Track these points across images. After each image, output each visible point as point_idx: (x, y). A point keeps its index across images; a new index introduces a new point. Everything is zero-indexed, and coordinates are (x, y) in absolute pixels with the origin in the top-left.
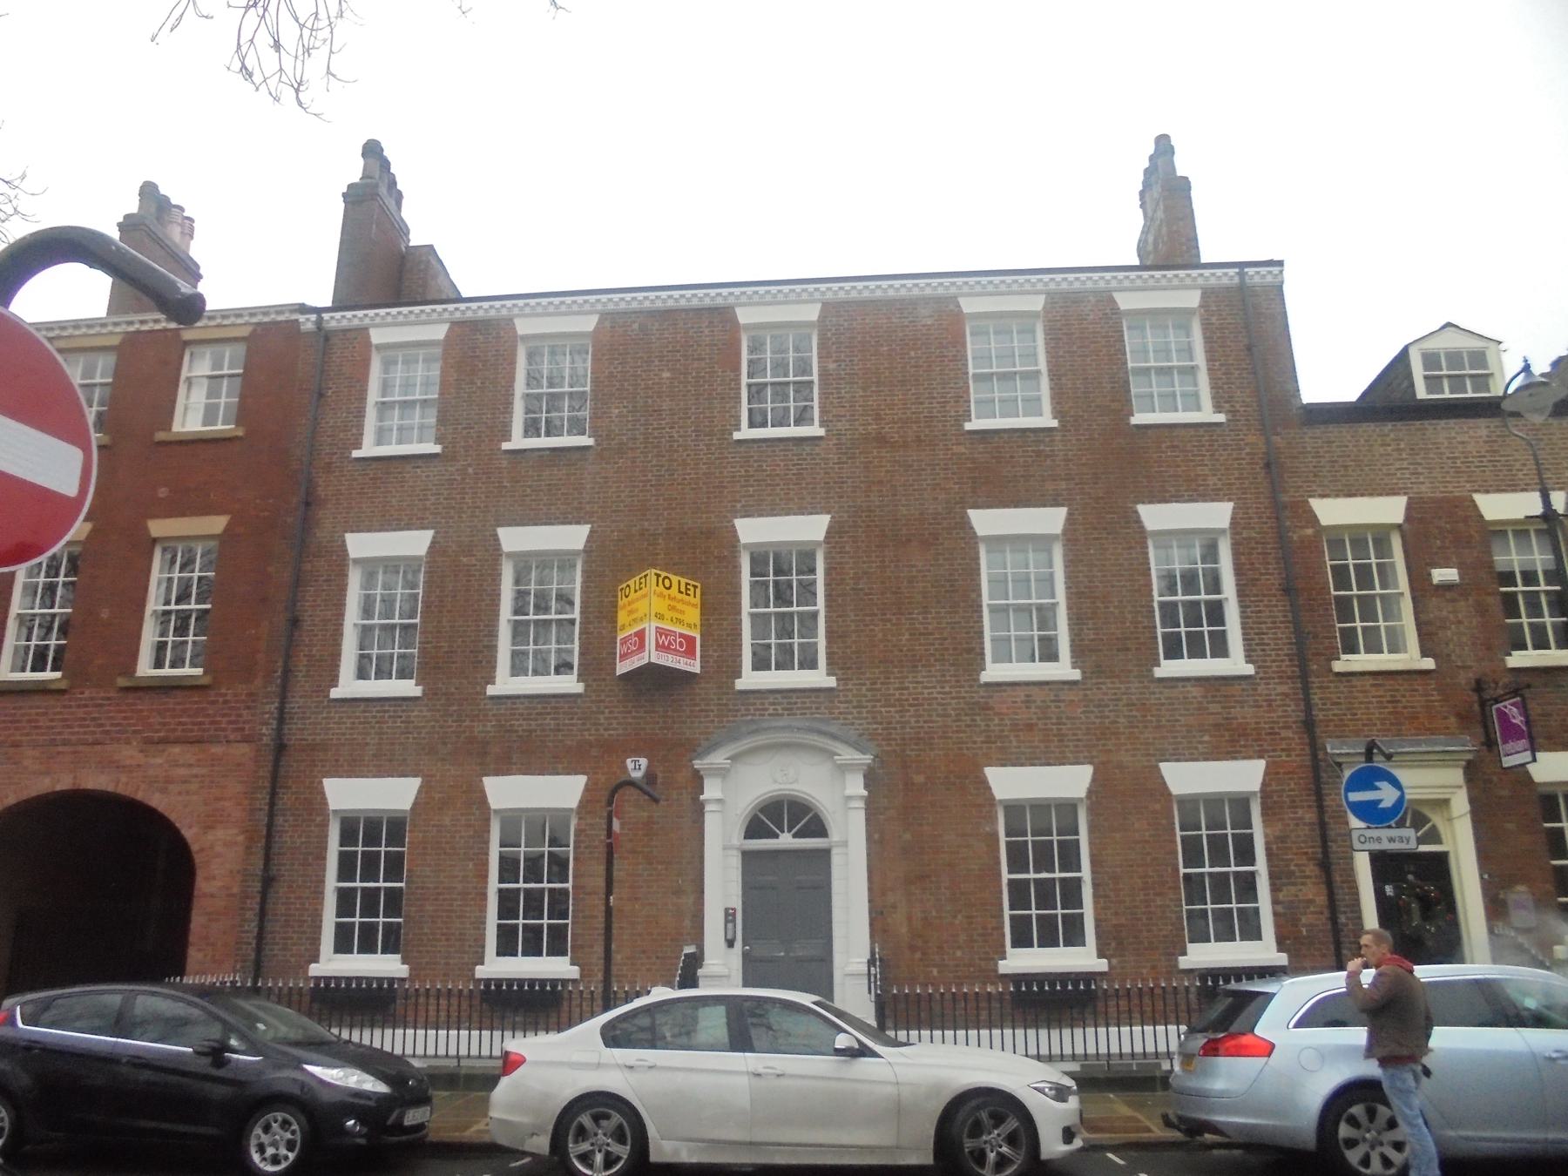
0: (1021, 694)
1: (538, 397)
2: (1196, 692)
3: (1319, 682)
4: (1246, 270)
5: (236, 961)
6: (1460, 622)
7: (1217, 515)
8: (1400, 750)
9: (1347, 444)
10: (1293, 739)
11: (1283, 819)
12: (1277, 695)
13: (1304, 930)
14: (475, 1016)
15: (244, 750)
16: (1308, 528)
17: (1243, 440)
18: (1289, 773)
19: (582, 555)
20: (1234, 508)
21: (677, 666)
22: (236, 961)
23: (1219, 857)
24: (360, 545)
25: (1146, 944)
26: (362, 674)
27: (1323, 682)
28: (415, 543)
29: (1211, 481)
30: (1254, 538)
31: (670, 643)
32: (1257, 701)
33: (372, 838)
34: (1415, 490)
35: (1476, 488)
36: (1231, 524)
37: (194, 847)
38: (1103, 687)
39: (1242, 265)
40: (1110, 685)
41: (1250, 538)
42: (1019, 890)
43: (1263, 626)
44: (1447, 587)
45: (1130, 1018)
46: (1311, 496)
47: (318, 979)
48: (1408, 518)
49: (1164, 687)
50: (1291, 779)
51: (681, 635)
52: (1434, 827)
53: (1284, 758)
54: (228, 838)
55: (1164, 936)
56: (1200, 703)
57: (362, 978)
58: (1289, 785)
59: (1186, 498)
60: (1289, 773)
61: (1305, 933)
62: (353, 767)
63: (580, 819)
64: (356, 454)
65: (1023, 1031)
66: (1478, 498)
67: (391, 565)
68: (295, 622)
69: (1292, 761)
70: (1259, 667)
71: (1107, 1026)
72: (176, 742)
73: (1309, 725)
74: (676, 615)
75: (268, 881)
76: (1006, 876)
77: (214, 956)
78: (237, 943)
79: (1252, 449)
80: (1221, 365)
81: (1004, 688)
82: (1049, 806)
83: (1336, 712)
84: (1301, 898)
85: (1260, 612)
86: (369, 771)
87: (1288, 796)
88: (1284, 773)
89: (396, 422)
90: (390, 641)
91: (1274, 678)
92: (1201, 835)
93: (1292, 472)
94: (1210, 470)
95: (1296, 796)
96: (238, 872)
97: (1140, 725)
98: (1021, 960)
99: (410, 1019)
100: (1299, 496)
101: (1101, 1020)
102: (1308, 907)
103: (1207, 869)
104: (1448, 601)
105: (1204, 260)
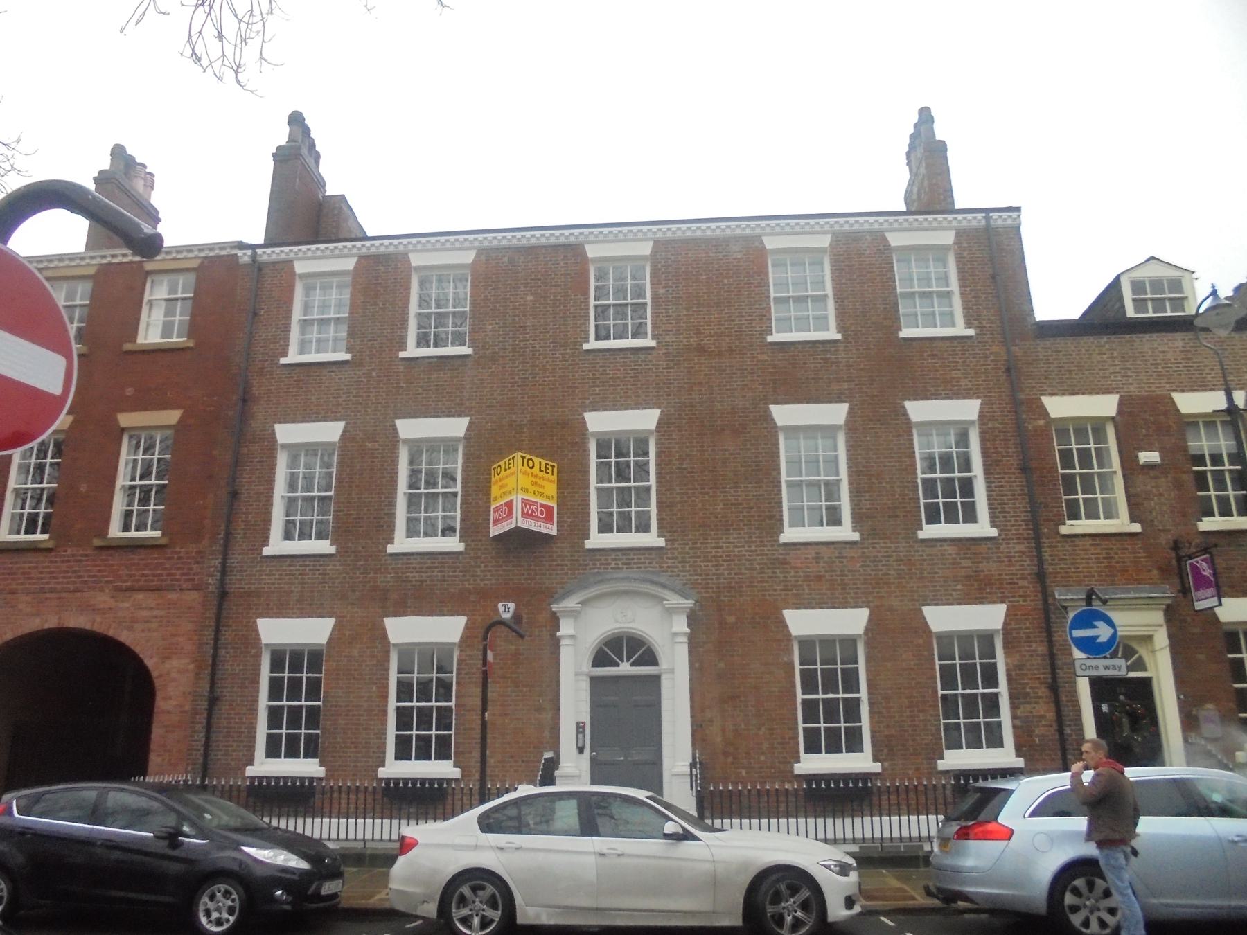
0: (812, 552)
1: (428, 316)
2: (951, 550)
3: (1049, 542)
4: (991, 215)
5: (188, 764)
6: (1161, 495)
7: (968, 409)
8: (1113, 596)
9: (1071, 353)
10: (1029, 587)
11: (1020, 651)
12: (1016, 552)
13: (1037, 739)
14: (378, 808)
15: (194, 596)
16: (1040, 420)
17: (988, 350)
18: (1025, 614)
19: (463, 441)
20: (981, 404)
21: (539, 530)
22: (188, 764)
23: (970, 681)
24: (286, 433)
25: (912, 751)
26: (288, 536)
27: (1052, 542)
28: (330, 431)
29: (963, 382)
30: (998, 428)
31: (533, 511)
32: (1000, 557)
33: (296, 666)
34: (1126, 390)
35: (1174, 388)
36: (979, 416)
37: (155, 674)
38: (877, 546)
39: (987, 211)
40: (882, 545)
41: (994, 428)
42: (810, 707)
43: (1005, 498)
44: (1150, 467)
45: (899, 810)
46: (1042, 395)
47: (253, 778)
48: (1120, 412)
49: (926, 546)
50: (1026, 619)
51: (542, 505)
52: (1140, 658)
53: (1021, 603)
54: (182, 666)
55: (926, 744)
56: (954, 559)
57: (288, 778)
58: (1025, 624)
59: (943, 396)
60: (1025, 614)
61: (1038, 742)
62: (281, 610)
63: (461, 651)
64: (283, 361)
65: (814, 820)
66: (1175, 396)
67: (311, 449)
68: (235, 495)
69: (1027, 605)
70: (1001, 530)
71: (881, 815)
72: (140, 590)
73: (1041, 576)
74: (537, 489)
75: (213, 701)
76: (800, 696)
77: (170, 760)
78: (188, 750)
79: (995, 357)
80: (971, 290)
81: (799, 547)
82: (834, 641)
83: (1062, 566)
84: (1035, 714)
85: (1002, 486)
86: (293, 613)
87: (1024, 633)
88: (1022, 615)
89: (315, 335)
90: (310, 510)
91: (1013, 539)
92: (955, 664)
93: (1028, 376)
94: (962, 374)
95: (1031, 633)
96: (190, 693)
97: (907, 576)
98: (812, 764)
99: (326, 810)
100: (1033, 394)
101: (875, 811)
102: (1041, 721)
103: (960, 691)
104: (1152, 478)
105: (957, 206)
